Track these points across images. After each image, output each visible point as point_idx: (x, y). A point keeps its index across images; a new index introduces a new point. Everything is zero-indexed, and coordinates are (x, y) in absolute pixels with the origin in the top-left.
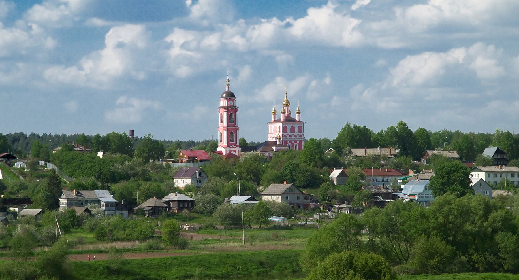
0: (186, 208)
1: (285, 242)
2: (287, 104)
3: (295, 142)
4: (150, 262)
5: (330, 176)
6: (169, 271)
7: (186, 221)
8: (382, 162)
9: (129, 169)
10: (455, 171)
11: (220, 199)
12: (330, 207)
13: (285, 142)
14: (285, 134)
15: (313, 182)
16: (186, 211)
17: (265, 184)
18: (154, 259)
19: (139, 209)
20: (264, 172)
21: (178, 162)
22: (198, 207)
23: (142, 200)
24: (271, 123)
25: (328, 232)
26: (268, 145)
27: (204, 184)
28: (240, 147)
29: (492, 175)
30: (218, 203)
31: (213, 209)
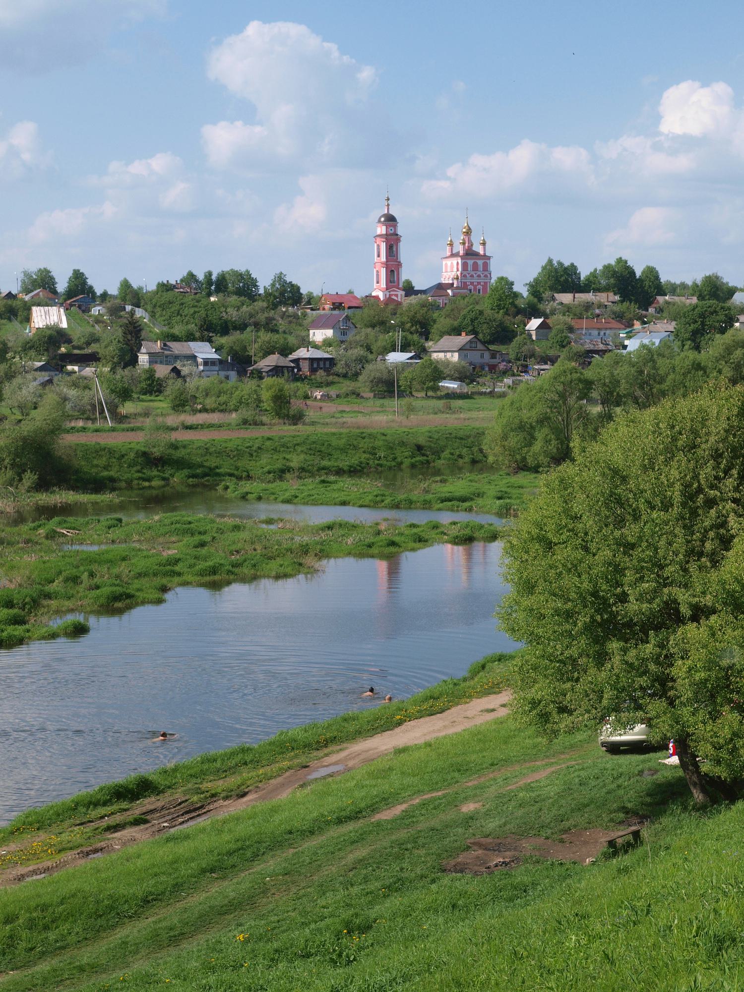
1: (462, 416)
2: (468, 232)
4: (224, 445)
5: (527, 328)
6: (256, 461)
8: (597, 311)
10: (712, 313)
11: (370, 356)
12: (525, 369)
15: (504, 335)
16: (321, 373)
18: (231, 440)
20: (435, 321)
21: (319, 309)
22: (339, 368)
25: (533, 393)
26: (441, 288)
27: (350, 337)
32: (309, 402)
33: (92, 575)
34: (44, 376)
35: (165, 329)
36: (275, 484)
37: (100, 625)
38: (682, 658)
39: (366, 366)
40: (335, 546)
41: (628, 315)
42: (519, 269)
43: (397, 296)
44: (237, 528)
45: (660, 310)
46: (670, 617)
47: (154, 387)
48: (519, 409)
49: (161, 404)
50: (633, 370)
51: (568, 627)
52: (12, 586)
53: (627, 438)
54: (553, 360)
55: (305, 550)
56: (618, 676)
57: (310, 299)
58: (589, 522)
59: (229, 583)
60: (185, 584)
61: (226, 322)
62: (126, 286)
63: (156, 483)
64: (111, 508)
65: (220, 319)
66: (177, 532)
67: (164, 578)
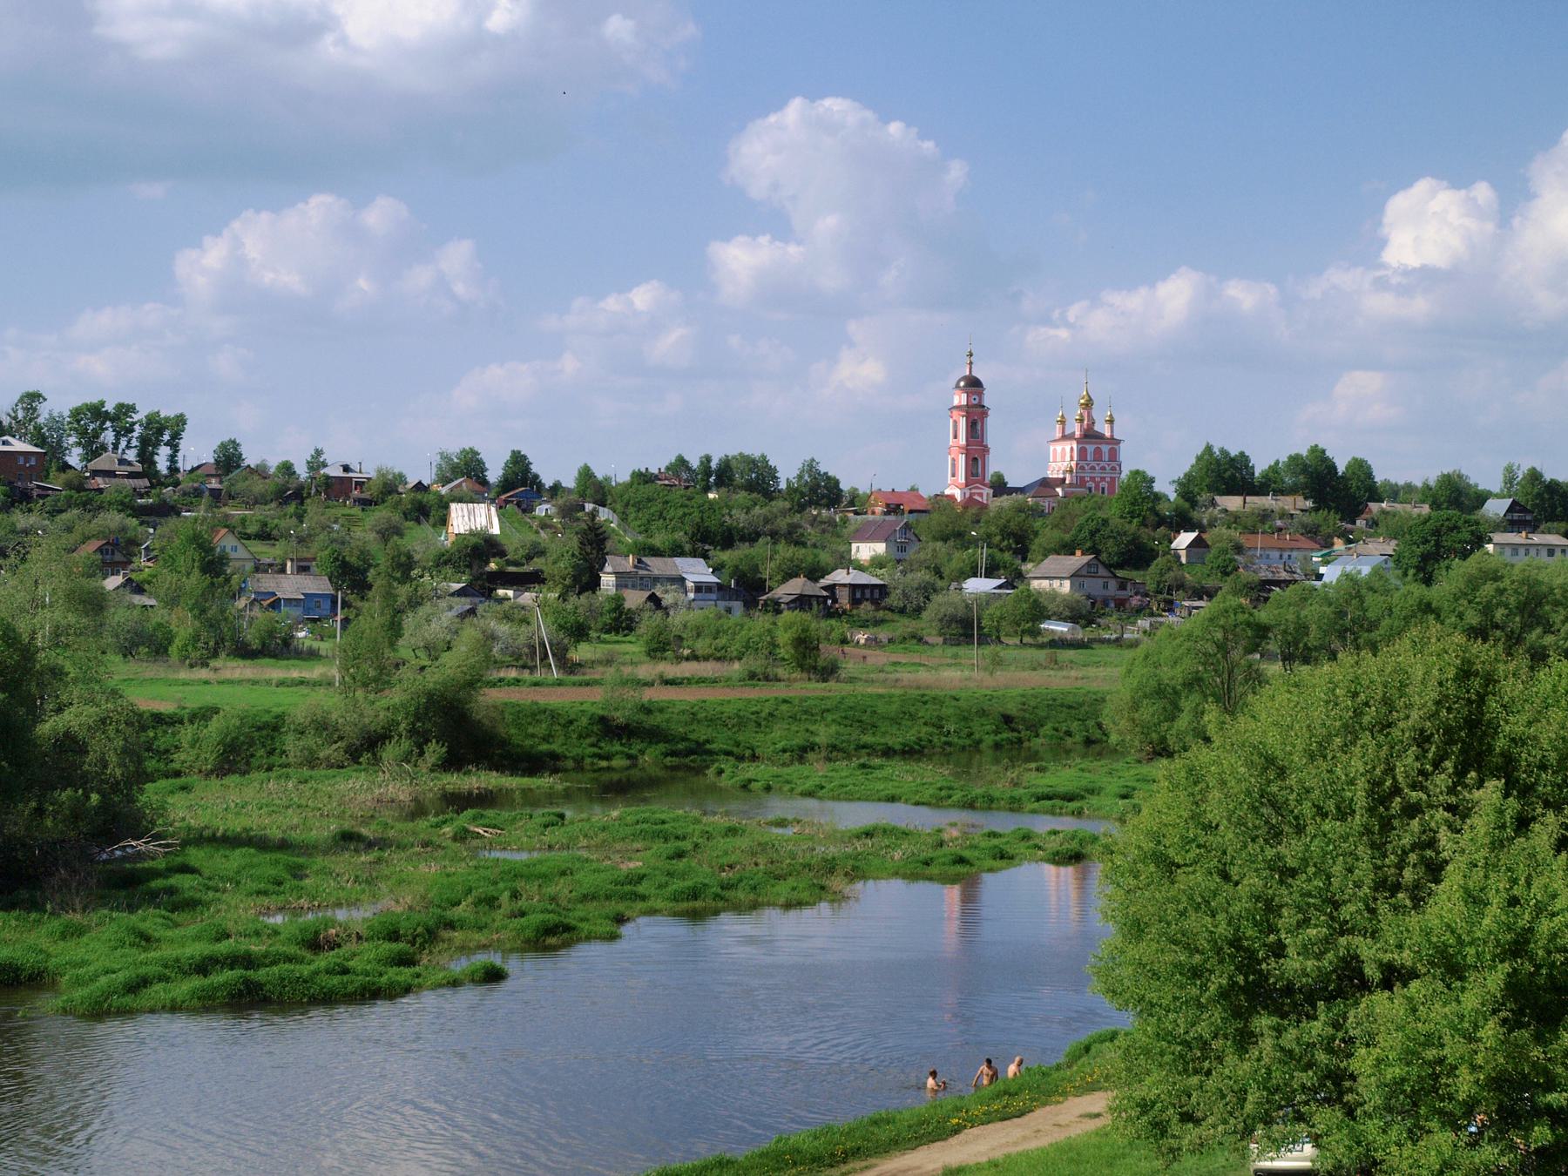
1: (1073, 673)
2: (1088, 404)
4: (719, 709)
5: (1173, 546)
8: (1279, 523)
10: (1451, 529)
11: (940, 584)
12: (1170, 607)
13: (1082, 479)
15: (1138, 556)
16: (866, 608)
20: (1036, 534)
22: (894, 600)
25: (1178, 641)
26: (1046, 484)
27: (912, 553)
29: (1508, 551)
32: (846, 648)
33: (515, 895)
34: (464, 604)
35: (641, 538)
36: (792, 768)
37: (524, 971)
38: (1368, 1045)
39: (934, 597)
40: (876, 862)
41: (1325, 530)
42: (1161, 459)
43: (981, 495)
44: (732, 831)
45: (1374, 523)
46: (1349, 981)
47: (622, 622)
48: (1157, 665)
49: (632, 647)
50: (1328, 610)
51: (1195, 991)
52: (399, 910)
53: (1288, 706)
54: (1210, 594)
55: (830, 867)
56: (1268, 1068)
57: (854, 498)
58: (1228, 836)
59: (716, 913)
60: (652, 912)
61: (729, 530)
62: (586, 475)
63: (618, 762)
64: (550, 797)
65: (722, 525)
66: (643, 834)
67: (623, 902)
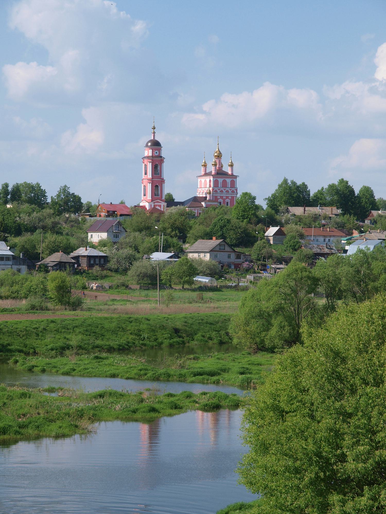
0: (97, 264)
1: (212, 305)
3: (227, 197)
4: (15, 326)
5: (266, 234)
7: (97, 280)
8: (323, 222)
9: (37, 222)
11: (138, 255)
12: (264, 268)
13: (216, 197)
14: (216, 189)
16: (97, 269)
17: (192, 241)
18: (21, 322)
19: (41, 264)
20: (191, 228)
21: (96, 216)
22: (112, 264)
23: (47, 254)
24: (201, 176)
25: (270, 287)
26: (196, 200)
27: (121, 239)
28: (165, 202)
30: (135, 259)
31: (129, 266)
